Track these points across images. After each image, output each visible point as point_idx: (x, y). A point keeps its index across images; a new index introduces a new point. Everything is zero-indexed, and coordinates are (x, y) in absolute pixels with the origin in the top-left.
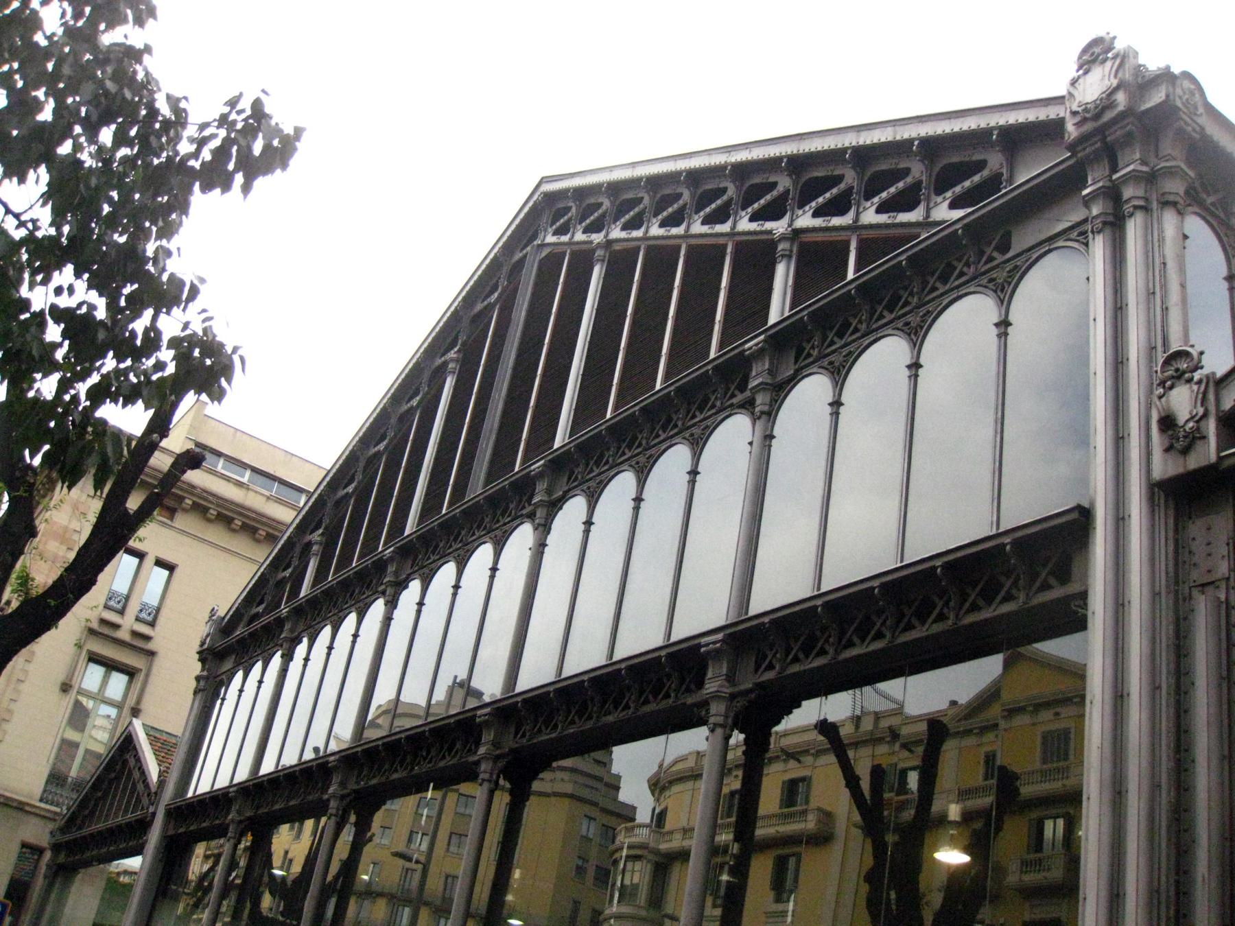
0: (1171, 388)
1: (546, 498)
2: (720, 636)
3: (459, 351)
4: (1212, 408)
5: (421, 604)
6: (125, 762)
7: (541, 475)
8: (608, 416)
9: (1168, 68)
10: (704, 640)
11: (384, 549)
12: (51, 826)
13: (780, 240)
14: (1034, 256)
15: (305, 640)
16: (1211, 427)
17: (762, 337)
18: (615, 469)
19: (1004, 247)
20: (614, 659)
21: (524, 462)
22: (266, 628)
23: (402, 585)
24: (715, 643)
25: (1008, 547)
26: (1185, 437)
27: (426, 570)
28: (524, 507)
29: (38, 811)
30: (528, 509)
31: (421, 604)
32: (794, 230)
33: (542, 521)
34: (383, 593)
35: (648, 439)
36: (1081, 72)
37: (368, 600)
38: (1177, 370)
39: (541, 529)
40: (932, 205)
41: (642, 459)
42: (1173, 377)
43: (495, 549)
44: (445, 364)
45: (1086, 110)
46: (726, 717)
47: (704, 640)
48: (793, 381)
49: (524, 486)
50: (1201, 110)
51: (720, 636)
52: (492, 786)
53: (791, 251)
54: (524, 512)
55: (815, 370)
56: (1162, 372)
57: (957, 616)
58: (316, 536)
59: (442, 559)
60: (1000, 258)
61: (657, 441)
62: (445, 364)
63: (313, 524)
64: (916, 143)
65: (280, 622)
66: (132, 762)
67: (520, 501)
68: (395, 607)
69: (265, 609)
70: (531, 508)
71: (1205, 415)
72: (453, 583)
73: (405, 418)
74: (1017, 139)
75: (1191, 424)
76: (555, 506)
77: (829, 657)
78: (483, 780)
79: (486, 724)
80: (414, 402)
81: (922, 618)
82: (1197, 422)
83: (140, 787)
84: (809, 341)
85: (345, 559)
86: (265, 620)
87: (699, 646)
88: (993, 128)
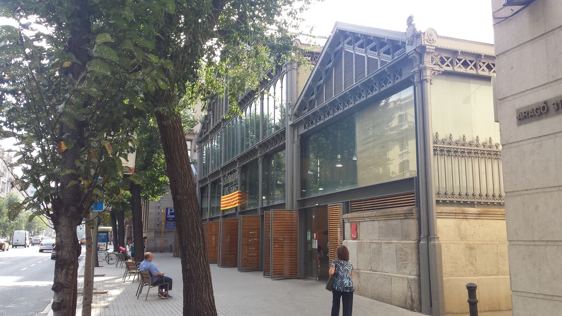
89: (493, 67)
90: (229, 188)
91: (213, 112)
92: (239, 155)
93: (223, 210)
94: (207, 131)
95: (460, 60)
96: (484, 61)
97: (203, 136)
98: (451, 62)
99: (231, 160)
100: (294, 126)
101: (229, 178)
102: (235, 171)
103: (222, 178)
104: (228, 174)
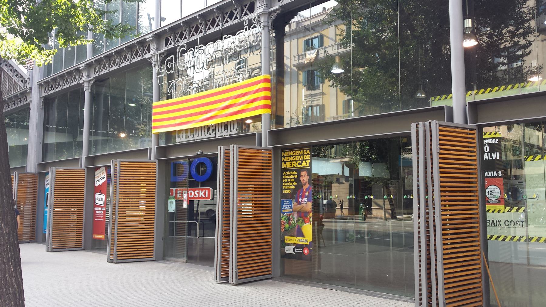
57: (241, 17)
92: (89, 57)
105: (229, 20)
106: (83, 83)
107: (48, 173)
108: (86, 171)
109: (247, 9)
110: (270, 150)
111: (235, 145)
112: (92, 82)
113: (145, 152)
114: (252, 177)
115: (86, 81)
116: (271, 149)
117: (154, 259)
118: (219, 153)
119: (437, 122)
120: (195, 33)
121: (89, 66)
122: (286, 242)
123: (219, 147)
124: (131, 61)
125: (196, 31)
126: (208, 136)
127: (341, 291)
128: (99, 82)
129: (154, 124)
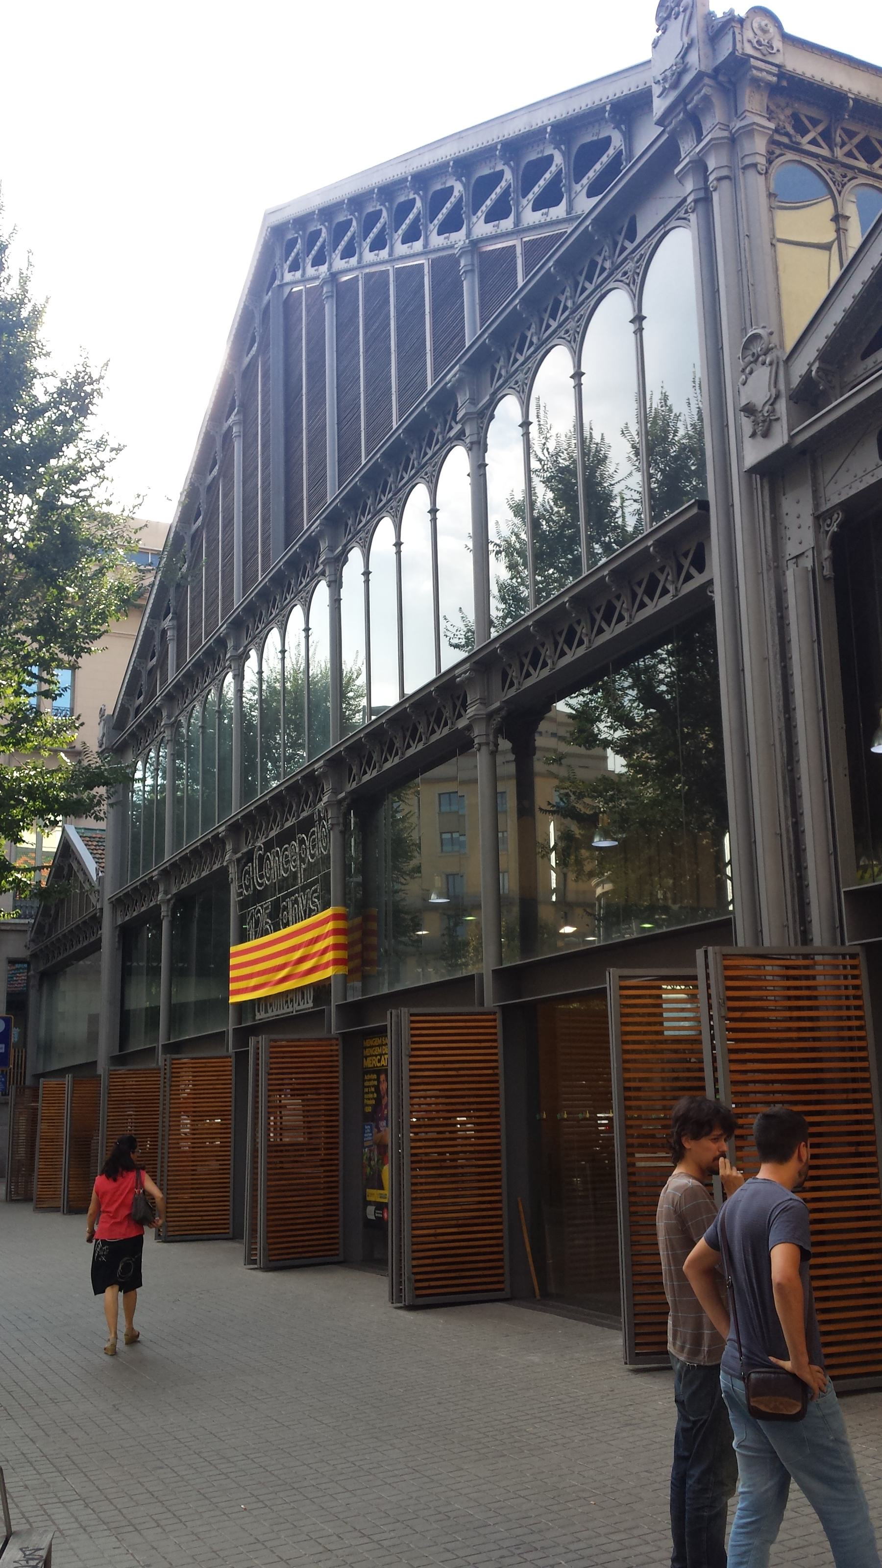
0: (751, 373)
1: (473, 409)
2: (467, 666)
3: (238, 413)
4: (782, 387)
5: (367, 573)
6: (70, 867)
7: (459, 384)
8: (520, 284)
9: (731, 12)
10: (457, 672)
11: (310, 525)
12: (28, 936)
13: (460, 256)
14: (593, 303)
15: (253, 653)
16: (782, 407)
17: (457, 367)
18: (543, 349)
19: (631, 235)
20: (442, 671)
21: (436, 373)
22: (149, 718)
23: (341, 560)
24: (465, 672)
25: (651, 549)
26: (764, 421)
27: (362, 535)
28: (451, 428)
29: (14, 928)
30: (457, 428)
31: (367, 573)
32: (471, 242)
33: (475, 438)
34: (323, 573)
35: (572, 297)
36: (660, 32)
37: (262, 635)
38: (753, 354)
39: (475, 447)
40: (573, 196)
41: (571, 325)
42: (751, 362)
43: (429, 488)
44: (230, 428)
45: (665, 79)
46: (487, 735)
47: (457, 672)
48: (493, 403)
49: (311, 547)
50: (777, 44)
51: (467, 666)
52: (492, 747)
53: (473, 265)
54: (452, 434)
55: (556, 341)
56: (744, 358)
57: (630, 616)
58: (167, 623)
59: (377, 518)
60: (630, 247)
61: (361, 525)
62: (230, 428)
63: (163, 613)
64: (549, 129)
65: (158, 710)
66: (75, 866)
67: (446, 422)
68: (341, 586)
69: (145, 699)
70: (459, 426)
71: (778, 396)
72: (362, 570)
73: (212, 488)
74: (628, 109)
75: (766, 408)
76: (485, 415)
77: (671, 594)
78: (480, 744)
79: (324, 775)
80: (215, 472)
81: (651, 594)
82: (772, 405)
83: (87, 887)
84: (599, 254)
85: (195, 645)
86: (148, 710)
87: (455, 677)
88: (605, 104)
89: (810, 126)
90: (274, 909)
91: (179, 617)
92: (236, 811)
93: (240, 1005)
94: (152, 694)
95: (851, 135)
96: (853, 127)
97: (132, 724)
98: (827, 136)
99: (201, 837)
100: (773, 473)
101: (274, 861)
102: (306, 825)
103: (233, 871)
104: (269, 846)
105: (646, 600)
106: (227, 866)
107: (382, 1031)
108: (499, 1016)
109: (602, 618)
110: (853, 956)
111: (710, 949)
112: (172, 902)
113: (222, 1035)
114: (475, 1072)
115: (163, 901)
116: (858, 950)
117: (230, 1236)
118: (388, 1023)
119: (717, 948)
120: (604, 626)
121: (235, 829)
122: (368, 1199)
123: (699, 953)
124: (360, 780)
125: (608, 619)
126: (286, 1010)
127: (534, 1309)
128: (183, 901)
129: (233, 986)
